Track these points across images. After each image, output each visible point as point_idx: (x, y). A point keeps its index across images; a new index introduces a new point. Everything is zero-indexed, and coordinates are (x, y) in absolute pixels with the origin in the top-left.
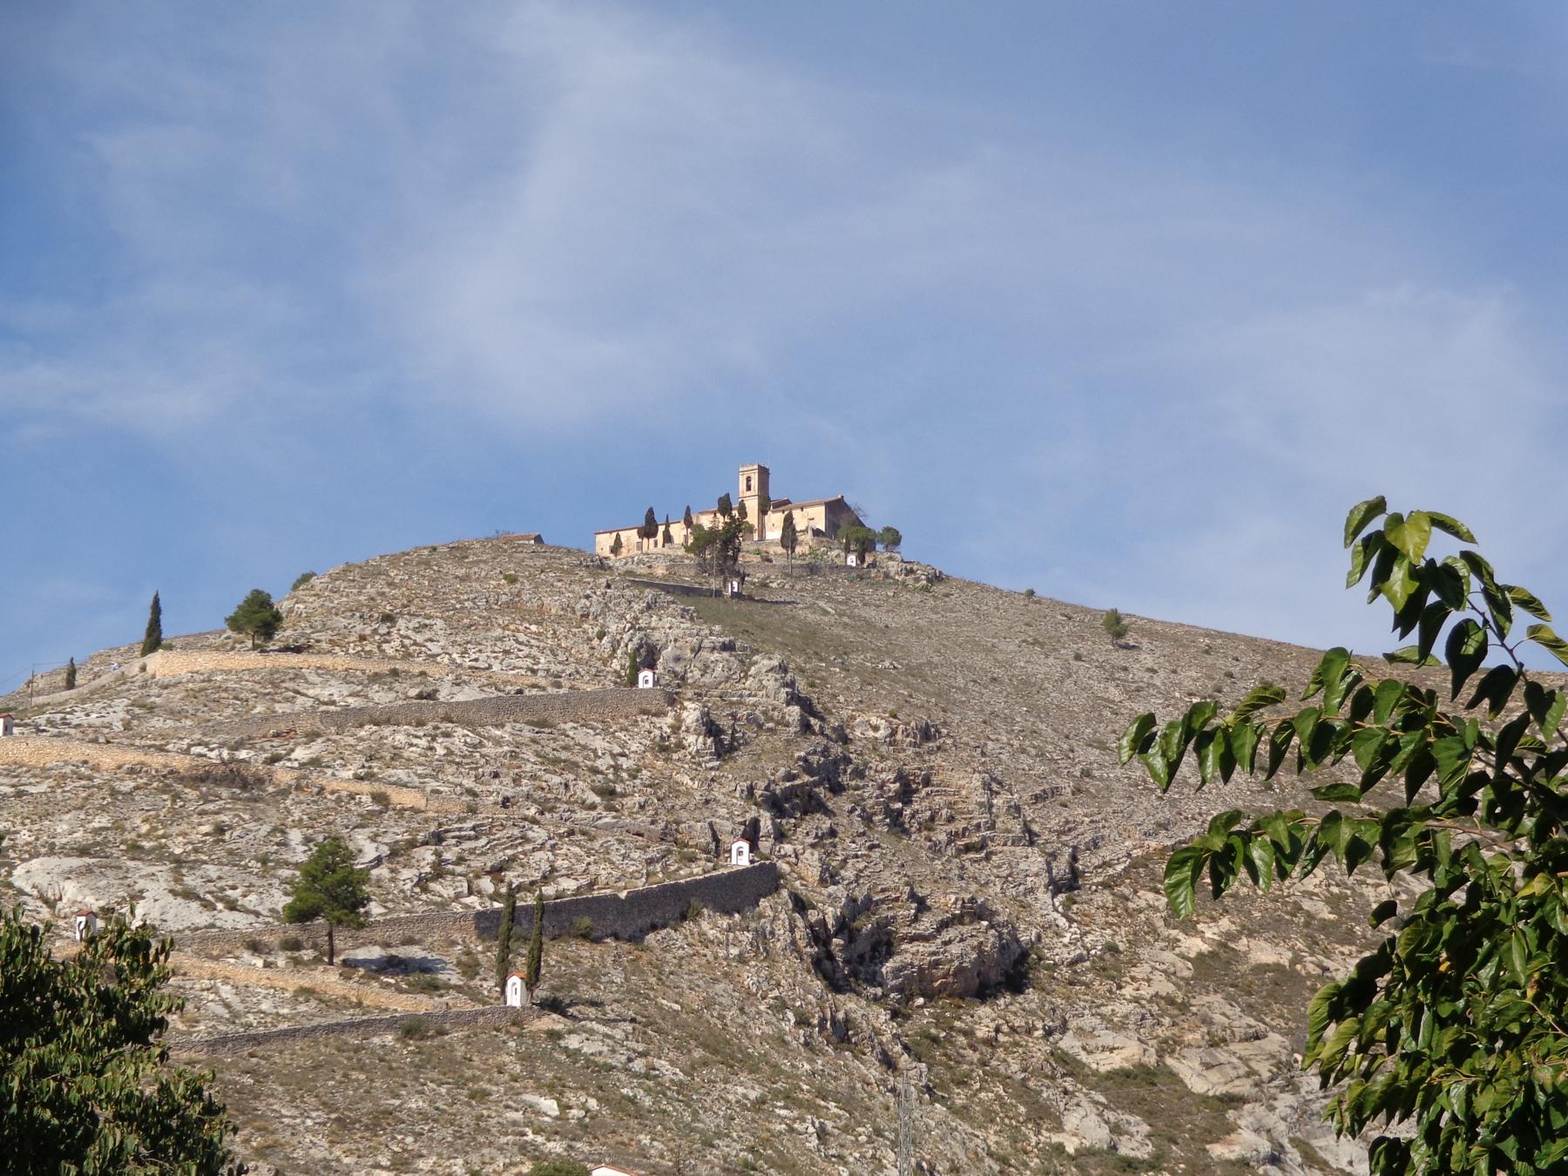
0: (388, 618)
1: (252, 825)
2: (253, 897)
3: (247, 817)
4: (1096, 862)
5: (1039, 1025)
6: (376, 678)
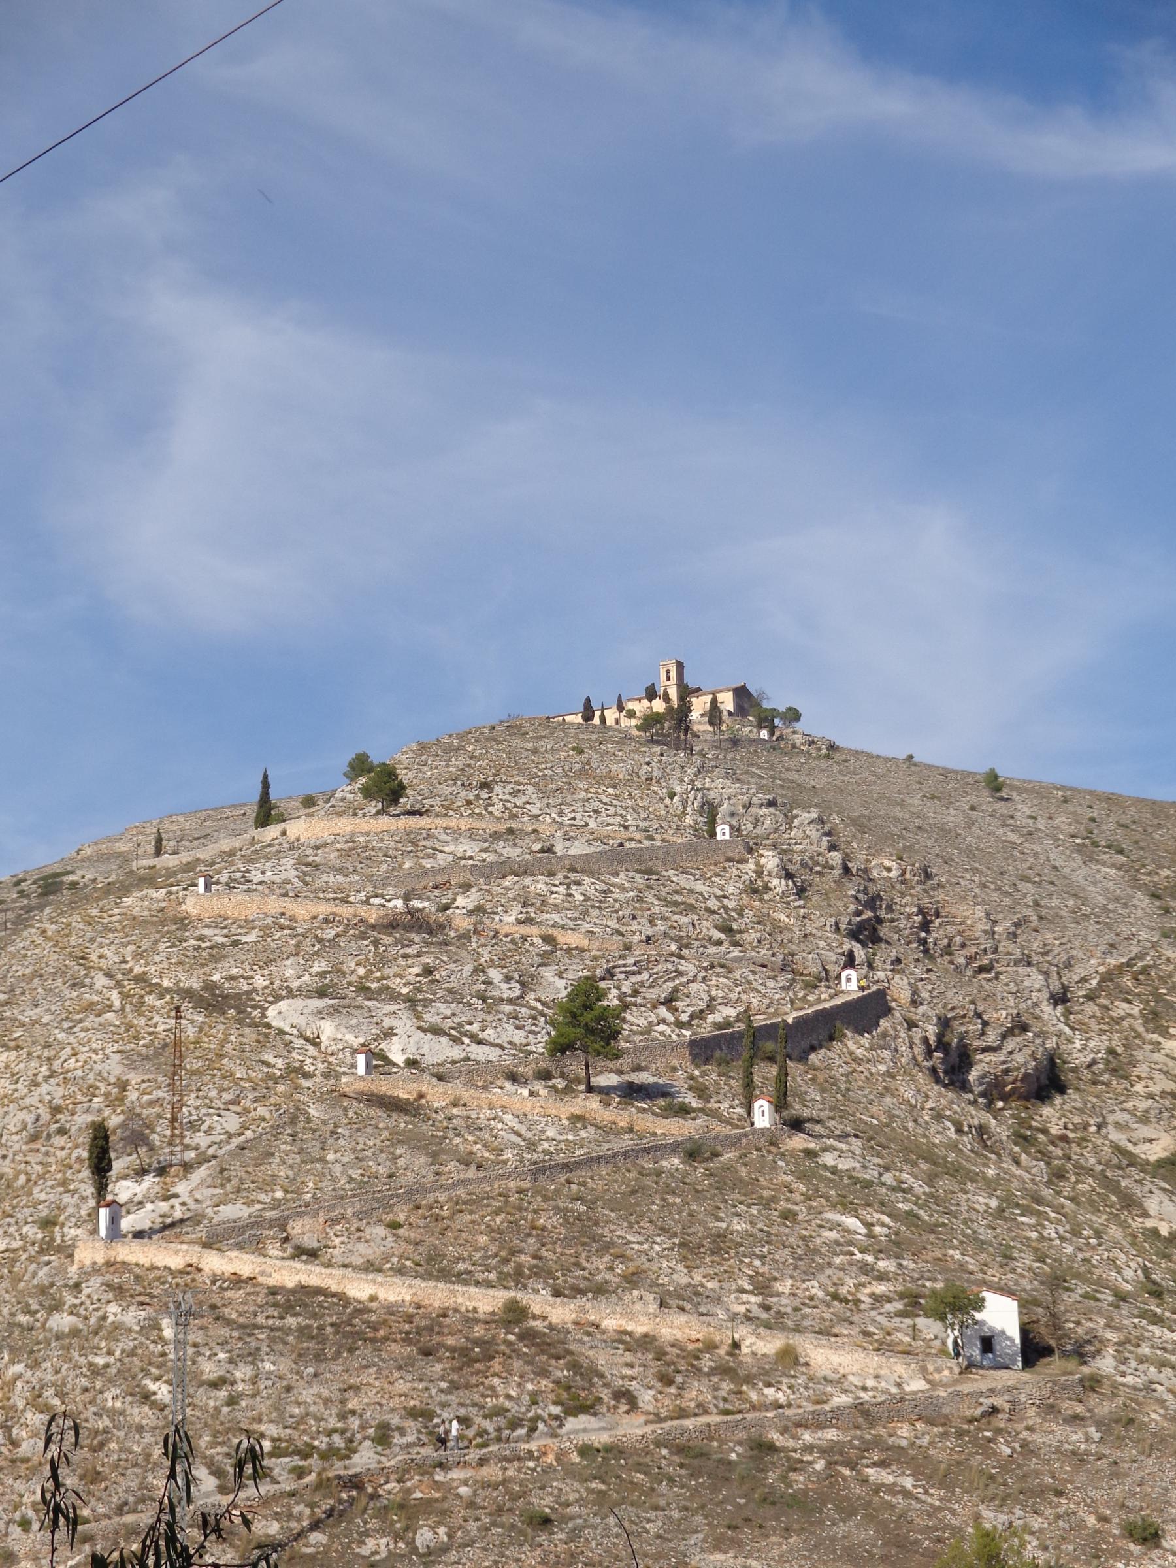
0: (485, 785)
1: (452, 966)
2: (490, 1031)
3: (445, 959)
4: (1076, 978)
5: (1092, 1122)
6: (496, 836)
